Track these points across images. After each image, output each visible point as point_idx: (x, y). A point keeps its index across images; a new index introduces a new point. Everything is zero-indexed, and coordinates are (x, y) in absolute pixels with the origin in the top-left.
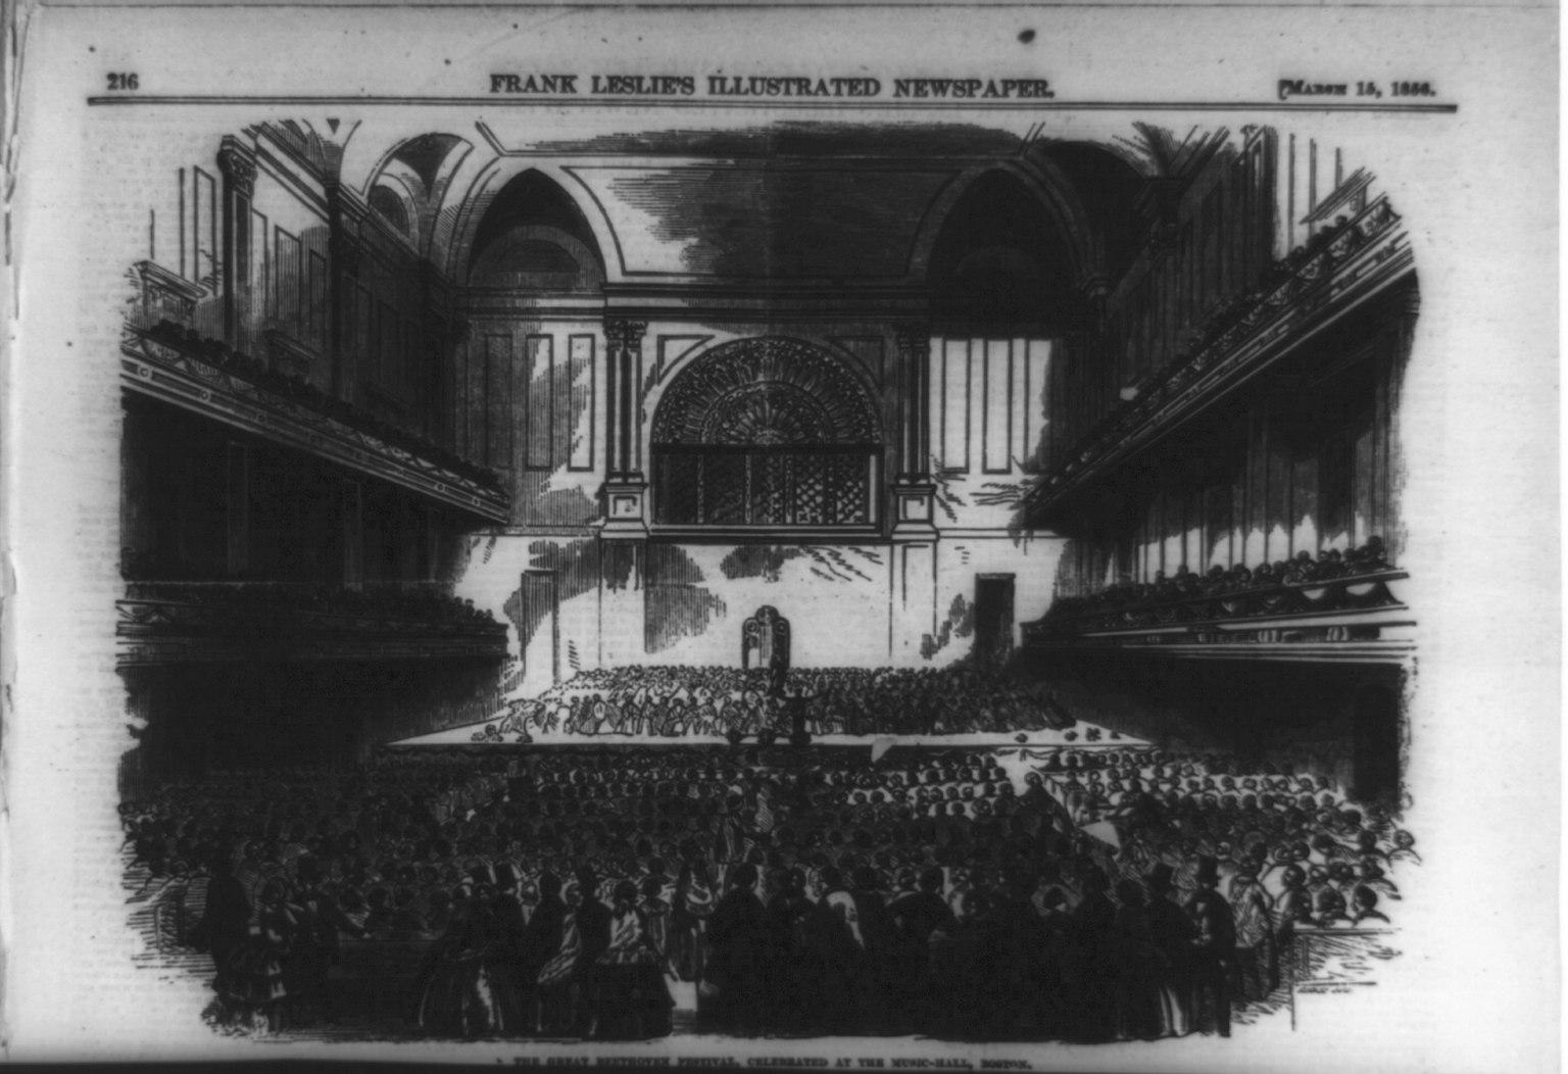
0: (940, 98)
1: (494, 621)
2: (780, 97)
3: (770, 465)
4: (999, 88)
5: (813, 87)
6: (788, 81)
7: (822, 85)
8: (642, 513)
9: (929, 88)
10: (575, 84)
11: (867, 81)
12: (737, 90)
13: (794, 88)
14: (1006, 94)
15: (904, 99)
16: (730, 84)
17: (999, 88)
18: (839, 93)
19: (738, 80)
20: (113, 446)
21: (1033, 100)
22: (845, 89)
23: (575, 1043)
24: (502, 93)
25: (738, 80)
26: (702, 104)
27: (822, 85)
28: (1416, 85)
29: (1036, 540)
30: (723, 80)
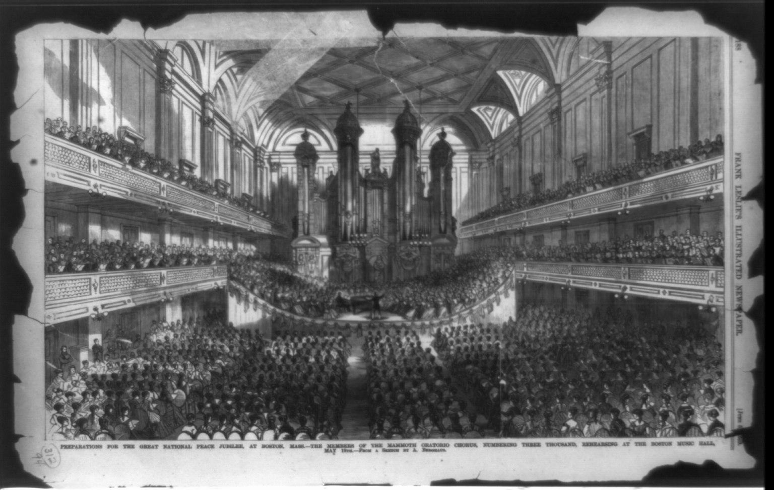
0: (735, 299)
1: (11, 161)
2: (735, 248)
3: (152, 363)
4: (739, 319)
5: (739, 258)
6: (741, 250)
7: (740, 261)
8: (651, 121)
9: (739, 296)
10: (739, 179)
11: (741, 275)
12: (737, 235)
13: (738, 252)
14: (737, 321)
15: (735, 288)
16: (739, 232)
17: (739, 319)
18: (737, 266)
19: (740, 235)
20: (14, 343)
21: (735, 329)
22: (738, 268)
23: (461, 38)
24: (735, 156)
25: (740, 235)
26: (732, 222)
27: (740, 261)
28: (738, 293)
29: (643, 125)
30: (740, 230)
